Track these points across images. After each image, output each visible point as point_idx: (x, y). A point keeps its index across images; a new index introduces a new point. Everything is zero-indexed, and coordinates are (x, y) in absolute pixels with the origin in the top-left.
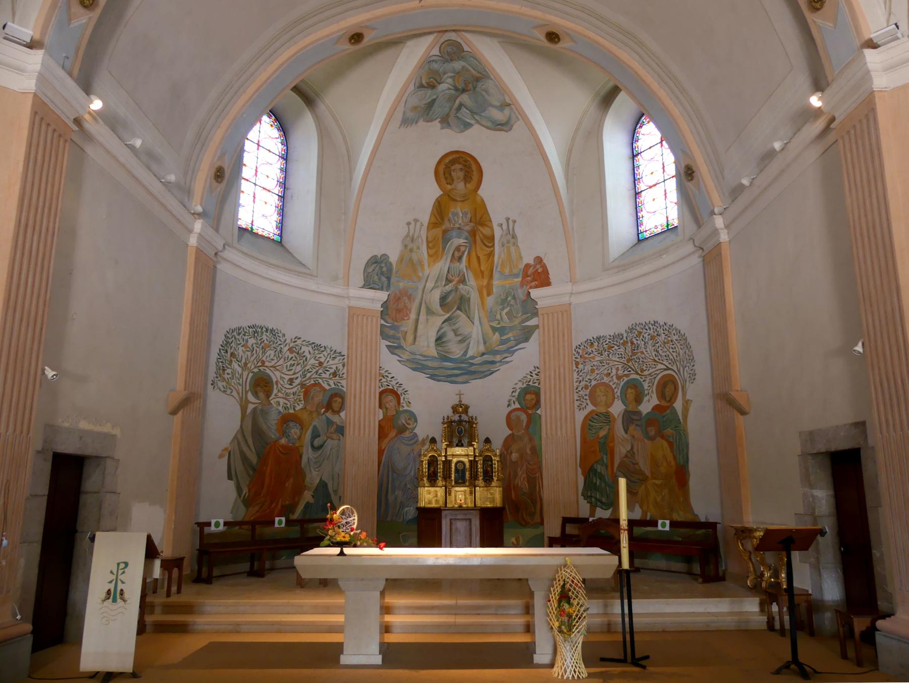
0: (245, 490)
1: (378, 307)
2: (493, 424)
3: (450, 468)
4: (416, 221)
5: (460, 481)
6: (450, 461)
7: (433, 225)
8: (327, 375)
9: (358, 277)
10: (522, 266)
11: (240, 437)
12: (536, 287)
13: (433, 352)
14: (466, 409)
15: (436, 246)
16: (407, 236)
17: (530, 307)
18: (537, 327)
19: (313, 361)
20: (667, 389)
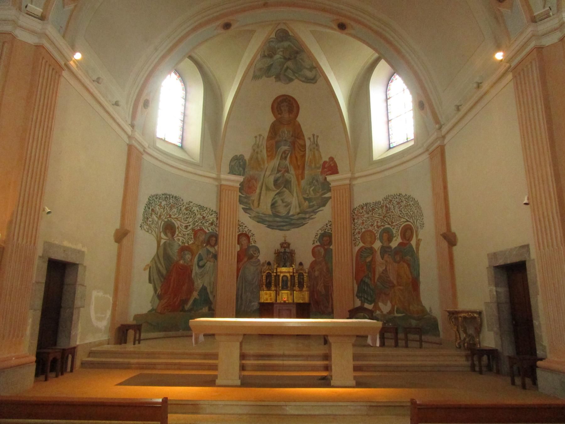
0: (159, 290)
1: (238, 185)
2: (304, 255)
3: (279, 279)
5: (285, 287)
6: (279, 276)
8: (207, 224)
9: (225, 167)
10: (322, 162)
11: (156, 259)
12: (331, 174)
13: (270, 212)
14: (289, 245)
15: (272, 151)
16: (255, 144)
17: (326, 187)
18: (330, 198)
19: (199, 216)
20: (407, 233)
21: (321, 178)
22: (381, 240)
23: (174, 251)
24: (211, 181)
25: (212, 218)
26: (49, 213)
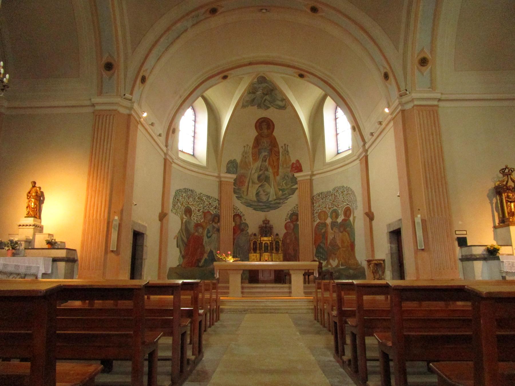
0: (183, 252)
1: (232, 181)
4: (247, 145)
5: (266, 250)
6: (262, 243)
7: (254, 147)
8: (212, 208)
9: (224, 169)
10: (291, 164)
12: (297, 172)
13: (255, 199)
14: (269, 221)
15: (256, 156)
16: (244, 152)
17: (294, 180)
18: (297, 188)
19: (207, 203)
21: (290, 175)
22: (331, 218)
23: (191, 227)
24: (214, 178)
25: (216, 204)
26: (136, 205)
